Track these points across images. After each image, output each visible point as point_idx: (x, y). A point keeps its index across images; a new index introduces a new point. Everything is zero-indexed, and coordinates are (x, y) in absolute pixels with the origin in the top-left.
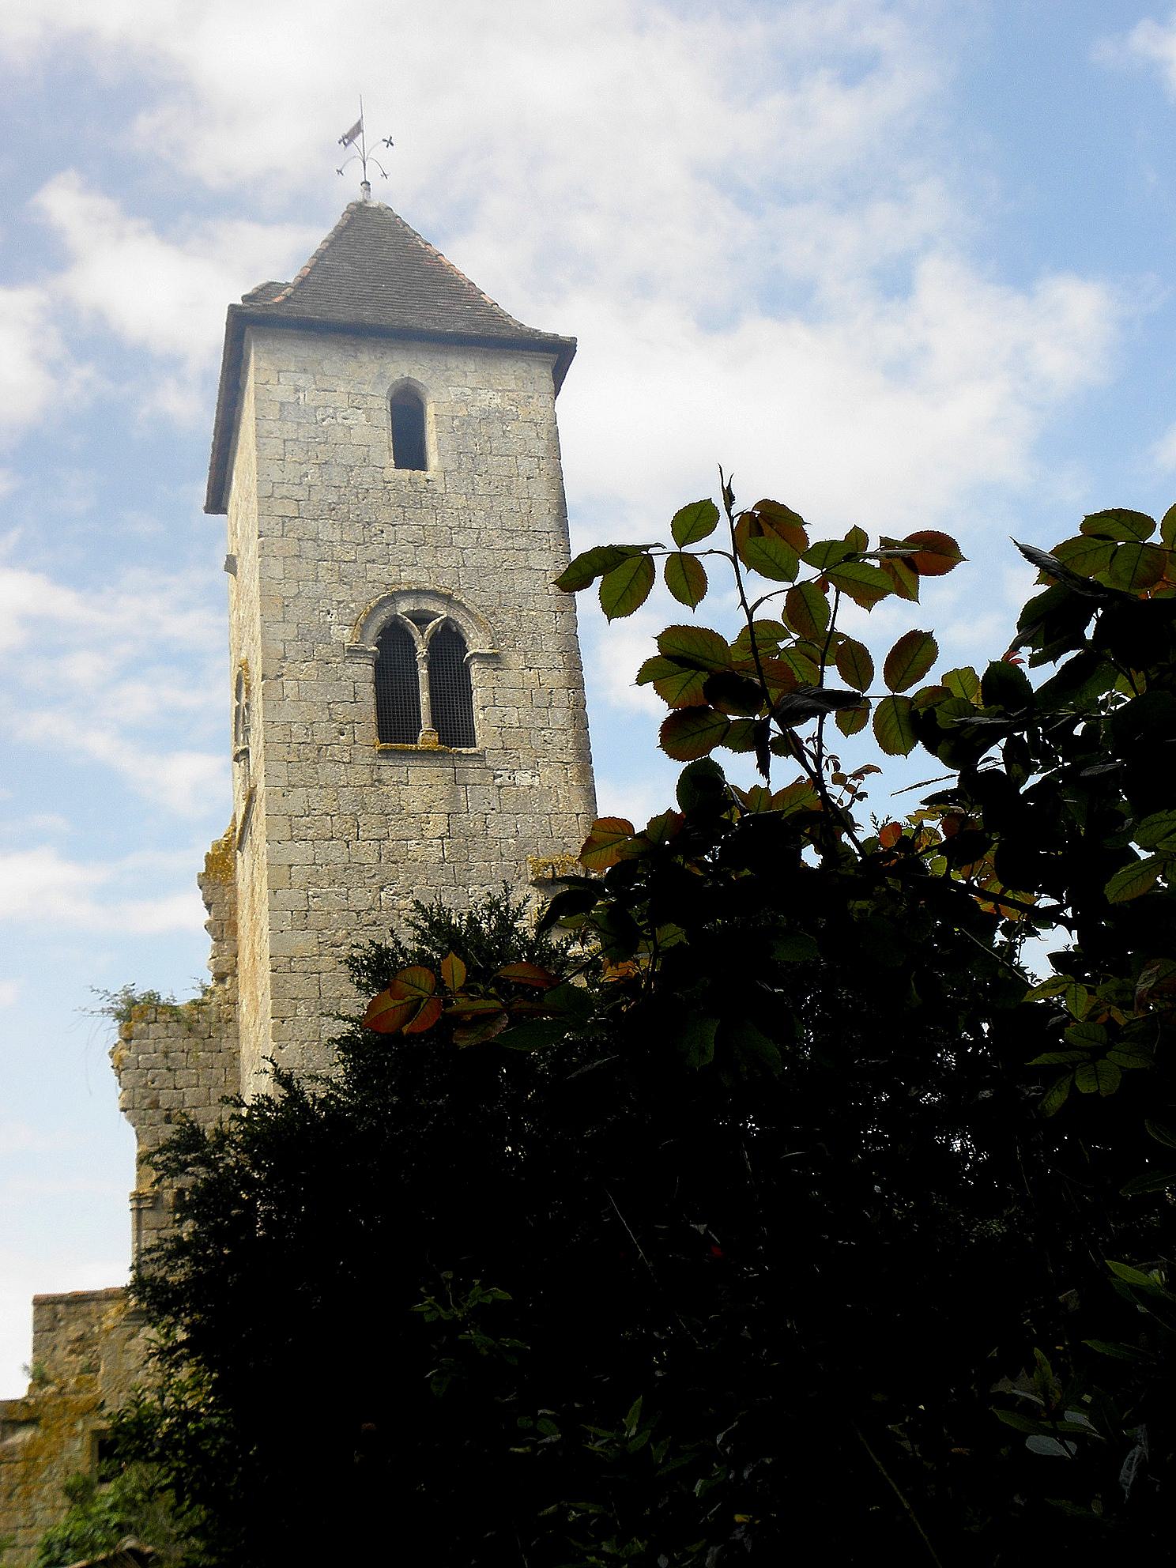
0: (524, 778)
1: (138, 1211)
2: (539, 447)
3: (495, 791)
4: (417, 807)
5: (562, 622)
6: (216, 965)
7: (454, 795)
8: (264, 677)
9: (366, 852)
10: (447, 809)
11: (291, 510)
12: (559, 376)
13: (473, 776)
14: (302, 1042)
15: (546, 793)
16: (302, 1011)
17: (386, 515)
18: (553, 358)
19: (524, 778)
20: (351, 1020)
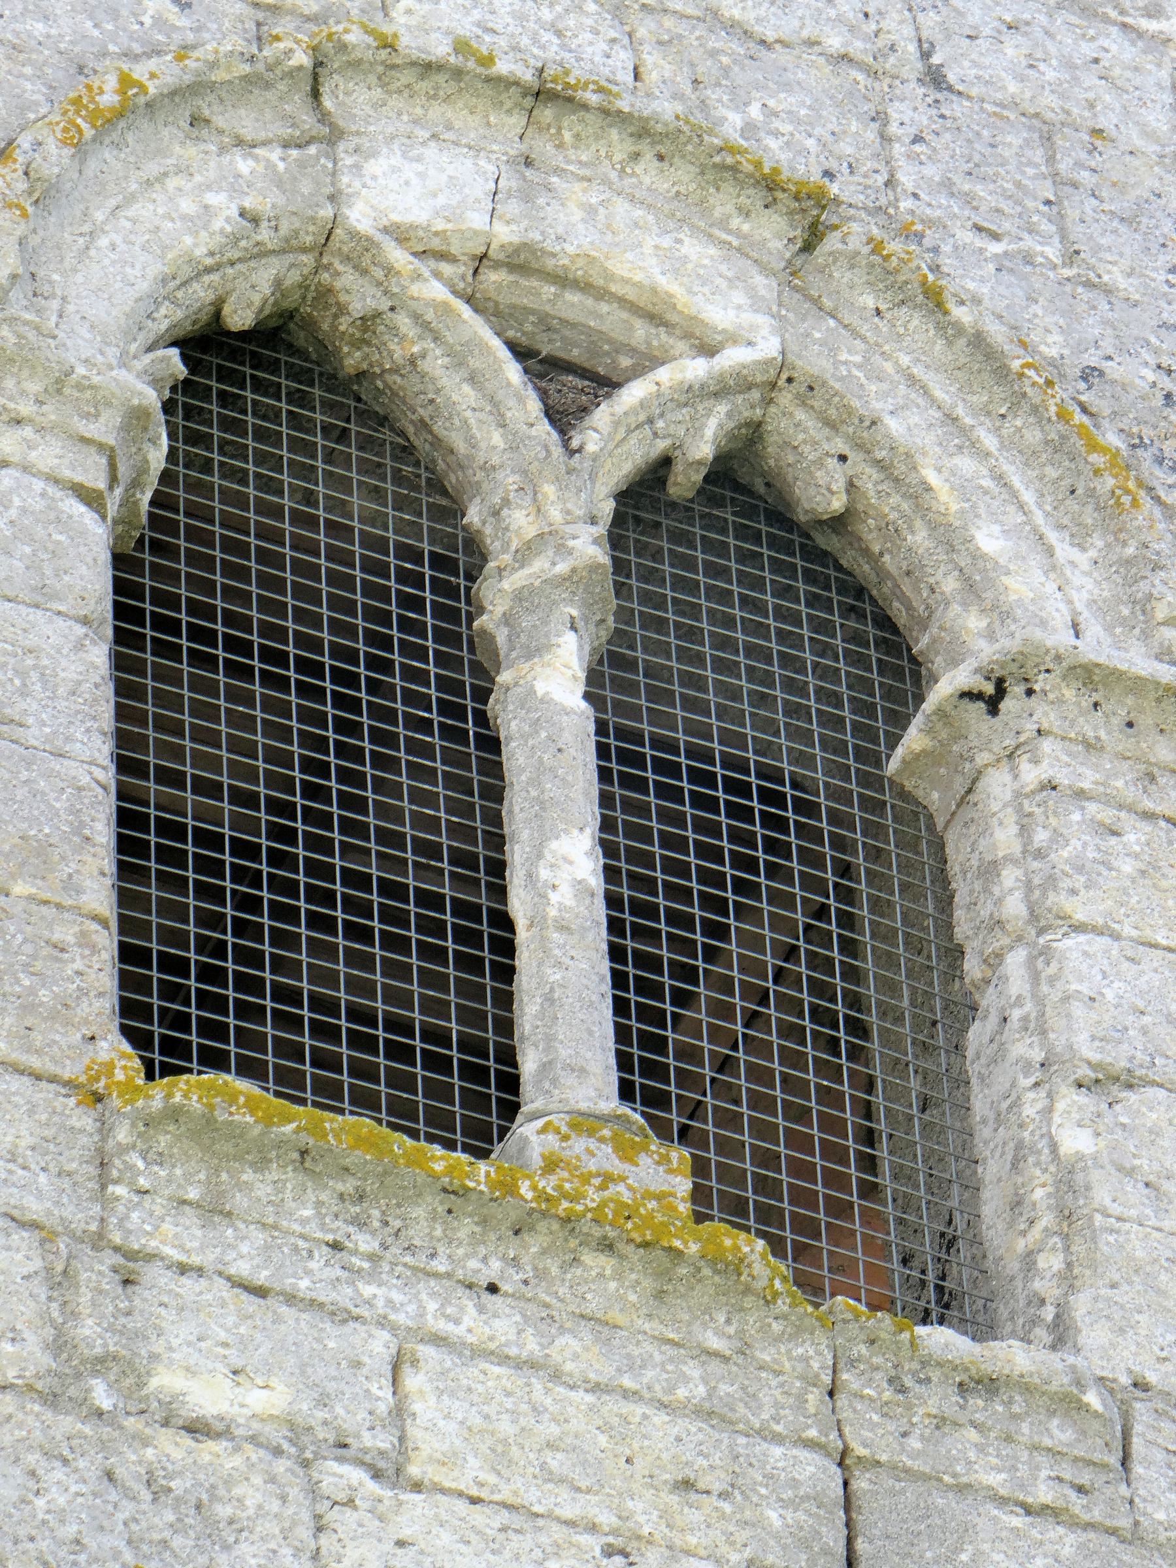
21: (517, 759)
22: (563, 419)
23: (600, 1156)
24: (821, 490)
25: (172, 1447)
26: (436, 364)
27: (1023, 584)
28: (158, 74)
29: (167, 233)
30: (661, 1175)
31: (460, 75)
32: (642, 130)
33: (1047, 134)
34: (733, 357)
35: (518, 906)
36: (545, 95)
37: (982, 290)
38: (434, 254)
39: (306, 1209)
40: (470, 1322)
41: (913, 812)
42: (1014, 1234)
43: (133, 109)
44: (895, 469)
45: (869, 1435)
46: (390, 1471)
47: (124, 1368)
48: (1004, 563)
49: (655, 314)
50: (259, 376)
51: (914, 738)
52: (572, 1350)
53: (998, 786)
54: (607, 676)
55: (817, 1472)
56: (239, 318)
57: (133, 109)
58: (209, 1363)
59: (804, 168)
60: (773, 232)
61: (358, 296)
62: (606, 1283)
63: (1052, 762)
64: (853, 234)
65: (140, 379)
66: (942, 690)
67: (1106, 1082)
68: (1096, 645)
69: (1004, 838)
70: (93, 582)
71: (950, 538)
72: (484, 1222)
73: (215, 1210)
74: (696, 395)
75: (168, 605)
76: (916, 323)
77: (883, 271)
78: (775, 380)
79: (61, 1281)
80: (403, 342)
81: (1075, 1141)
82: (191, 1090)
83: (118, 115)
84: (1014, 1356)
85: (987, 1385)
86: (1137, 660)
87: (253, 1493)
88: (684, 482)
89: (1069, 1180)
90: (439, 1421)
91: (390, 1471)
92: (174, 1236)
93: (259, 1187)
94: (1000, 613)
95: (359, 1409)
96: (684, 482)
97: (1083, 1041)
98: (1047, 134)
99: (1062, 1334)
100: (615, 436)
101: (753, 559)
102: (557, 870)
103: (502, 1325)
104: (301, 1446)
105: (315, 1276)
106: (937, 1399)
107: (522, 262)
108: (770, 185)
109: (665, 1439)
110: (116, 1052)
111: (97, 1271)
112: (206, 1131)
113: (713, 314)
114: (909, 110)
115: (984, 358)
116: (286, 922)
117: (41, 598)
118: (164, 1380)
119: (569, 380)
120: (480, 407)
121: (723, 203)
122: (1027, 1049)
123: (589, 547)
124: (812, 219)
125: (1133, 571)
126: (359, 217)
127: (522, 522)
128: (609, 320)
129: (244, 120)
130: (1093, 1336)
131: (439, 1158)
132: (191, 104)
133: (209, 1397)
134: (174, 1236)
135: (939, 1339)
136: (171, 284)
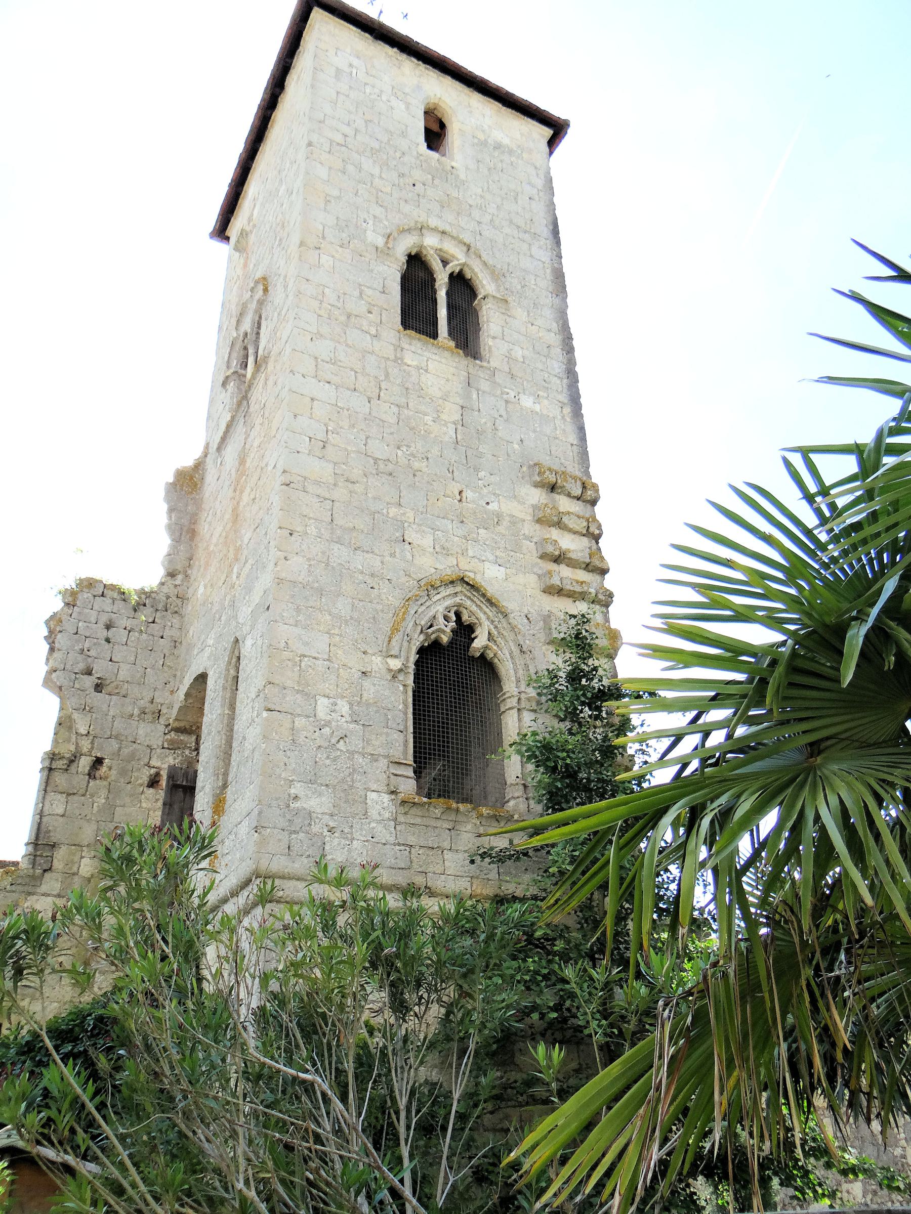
0: (527, 402)
1: (49, 770)
2: (540, 183)
3: (504, 404)
4: (435, 392)
5: (557, 301)
6: (170, 562)
7: (468, 397)
8: (302, 244)
9: (388, 413)
10: (461, 402)
11: (339, 138)
12: (552, 143)
13: (485, 386)
14: (309, 559)
15: (482, 1061)
16: (312, 530)
17: (417, 175)
18: (548, 132)
19: (527, 402)
20: (255, 905)
21: (439, 301)
22: (444, 266)
23: (446, 341)
24: (468, 276)
25: (406, 367)
26: (432, 260)
27: (487, 287)
28: (406, 227)
29: (405, 245)
30: (452, 344)
31: (435, 230)
32: (452, 237)
33: (491, 241)
34: (461, 262)
35: (438, 316)
36: (443, 233)
37: (485, 257)
38: (432, 248)
39: (419, 345)
40: (434, 357)
41: (475, 309)
42: (484, 352)
43: (404, 231)
44: (476, 274)
45: (471, 371)
46: (426, 371)
47: (402, 359)
48: (485, 285)
49: (453, 256)
50: (416, 261)
51: (476, 302)
52: (443, 360)
53: (484, 307)
54: (447, 294)
55: (466, 374)
56: (413, 254)
57: (404, 231)
58: (410, 359)
59: (468, 242)
60: (465, 249)
61: (424, 252)
62: (447, 354)
63: (490, 305)
64: (472, 250)
65: (404, 259)
66: (480, 297)
67: (494, 338)
68: (494, 294)
69: (485, 313)
70: (399, 280)
71: (481, 282)
72: (533, 1039)
73: (410, 344)
74: (457, 265)
75: (406, 280)
76: (478, 259)
77: (475, 253)
78: (464, 264)
79: (396, 350)
80: (429, 258)
81: (490, 343)
82: (408, 332)
83: (403, 231)
84: (485, 364)
85: (481, 367)
86: (498, 296)
87: (413, 372)
88: (455, 274)
89: (490, 347)
90: (431, 367)
91: (426, 371)
92: (406, 346)
93: (414, 342)
94: (485, 290)
95: (424, 365)
96: (455, 274)
97: (492, 333)
98: (491, 241)
99: (489, 362)
100: (449, 269)
101: (462, 284)
102: (442, 313)
103: (437, 357)
104: (418, 368)
105: (419, 351)
106: (477, 368)
107: (440, 250)
108: (465, 244)
109: (452, 370)
110: (401, 327)
111: (399, 350)
112: (410, 336)
113: (459, 258)
114: (478, 237)
115: (485, 264)
116: (416, 313)
117: (394, 281)
118: (405, 361)
119: (445, 263)
120: (436, 264)
121: (460, 245)
122: (486, 334)
123: (447, 280)
124: (469, 247)
125: (498, 287)
126: (425, 244)
127: (440, 277)
128: (448, 257)
129: (414, 233)
130: (492, 363)
131: (432, 340)
132: (409, 230)
133: (409, 363)
134: (406, 346)
135: (477, 362)
136: (408, 248)
